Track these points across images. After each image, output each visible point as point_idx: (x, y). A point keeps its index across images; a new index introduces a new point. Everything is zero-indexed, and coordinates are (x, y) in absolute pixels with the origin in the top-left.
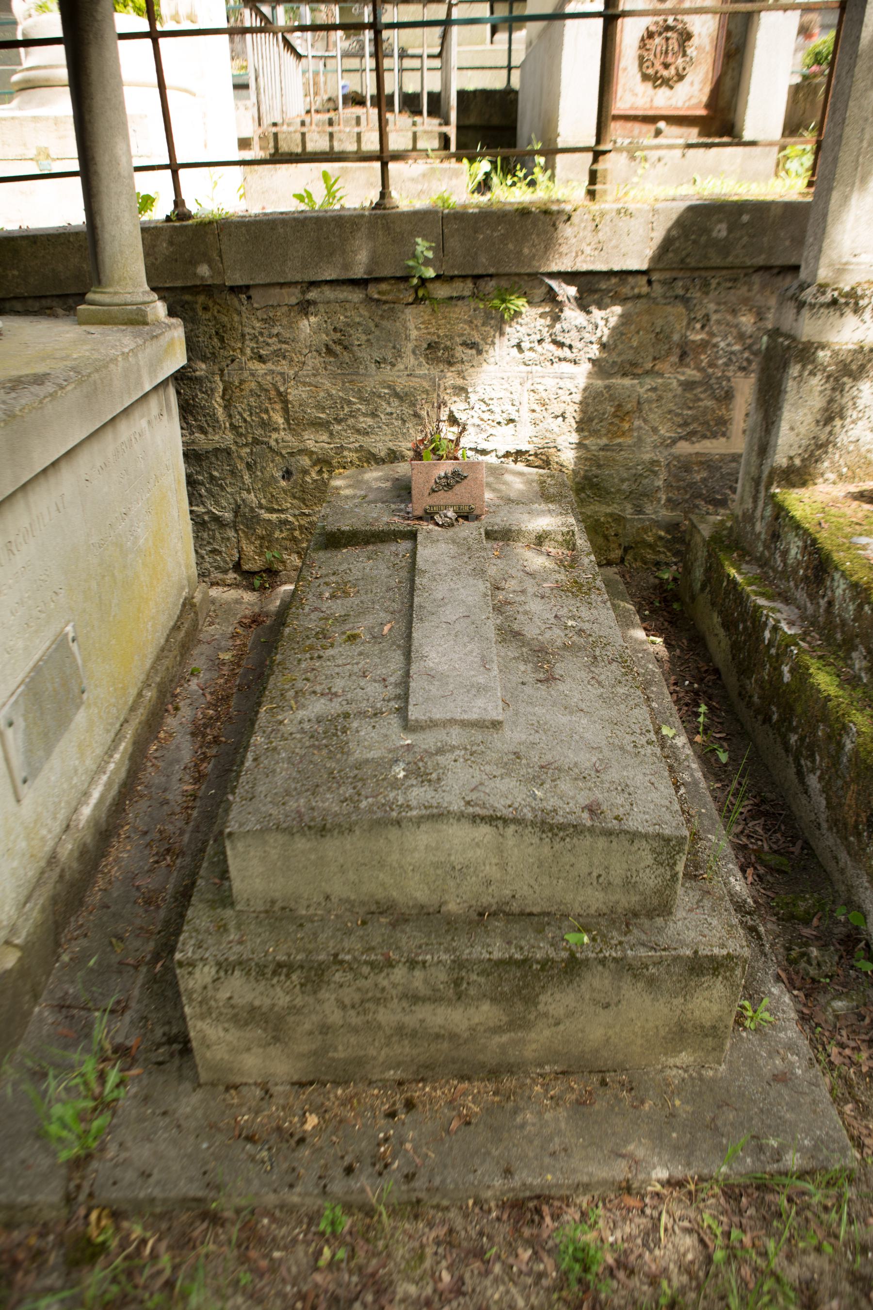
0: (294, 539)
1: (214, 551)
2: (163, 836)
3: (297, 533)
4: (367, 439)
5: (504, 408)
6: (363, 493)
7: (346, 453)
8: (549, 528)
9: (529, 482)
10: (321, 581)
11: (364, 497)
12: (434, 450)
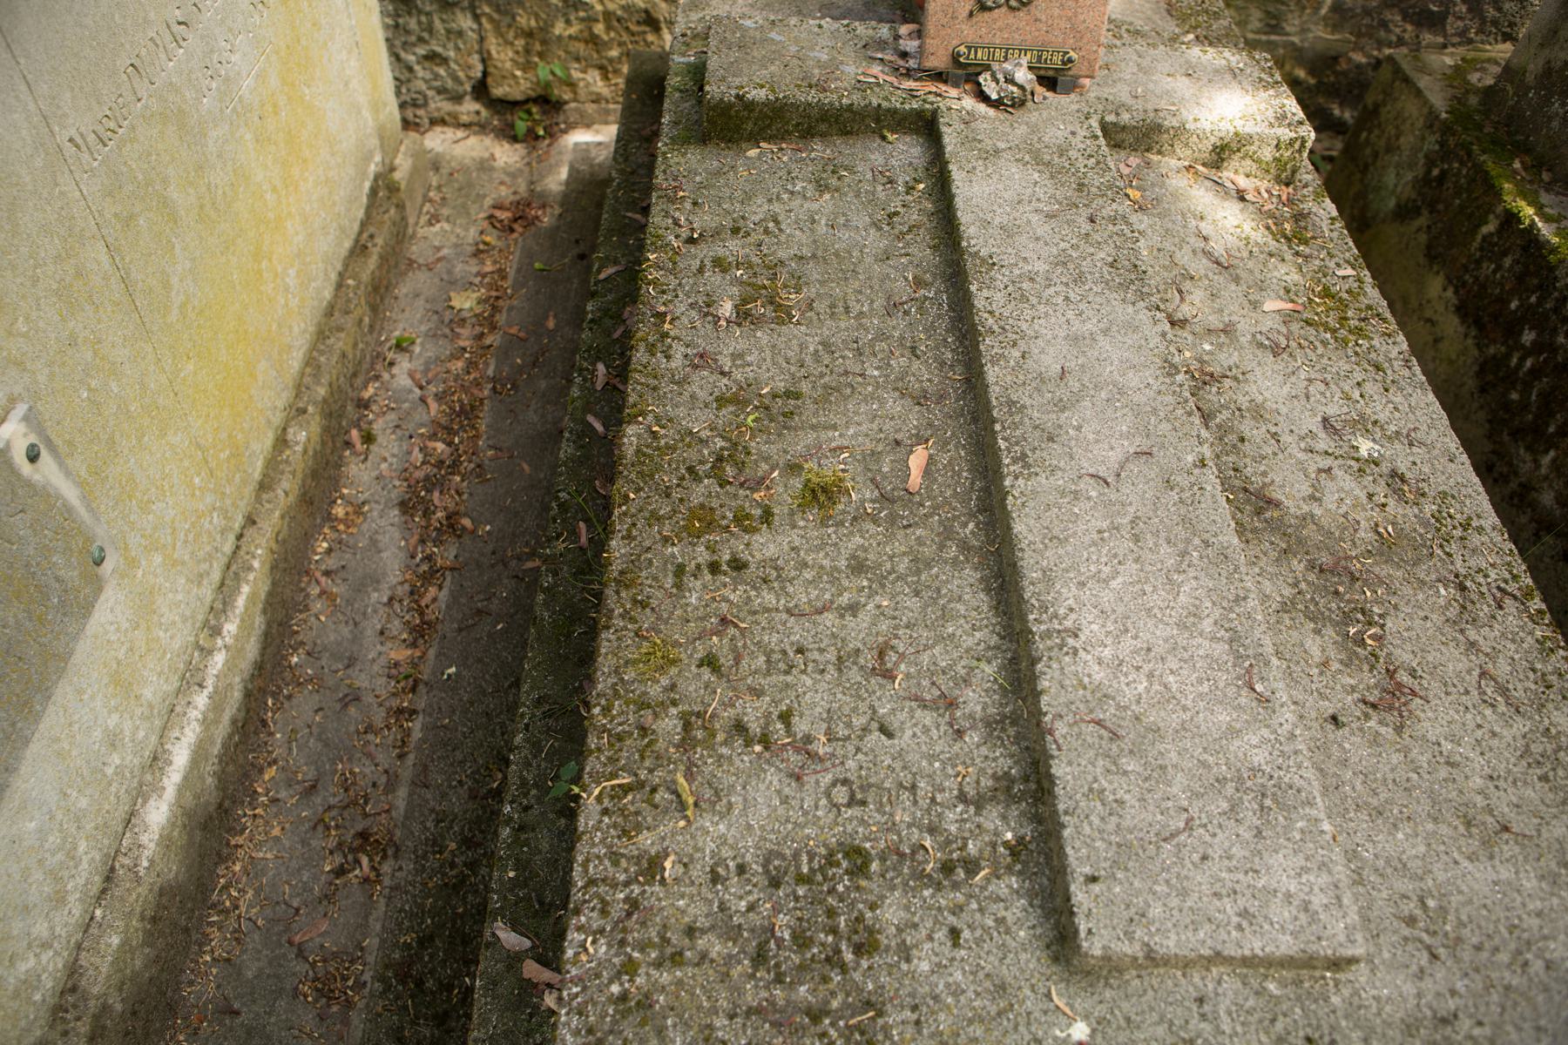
0: (593, 40)
1: (432, 57)
2: (355, 802)
3: (599, 29)
10: (704, 252)
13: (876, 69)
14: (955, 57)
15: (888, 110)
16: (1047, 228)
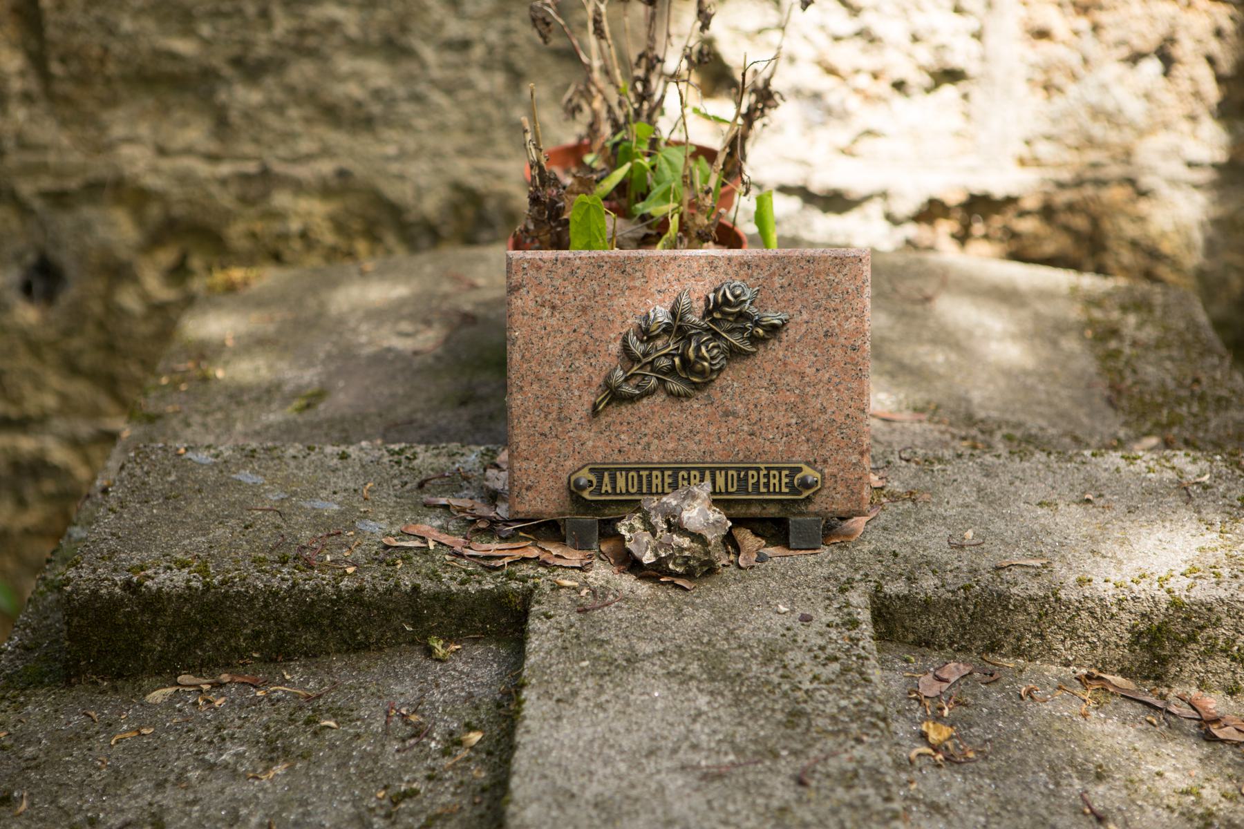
4: (365, 145)
5: (920, 22)
6: (310, 376)
7: (282, 199)
8: (1204, 591)
9: (1047, 332)
11: (313, 399)
12: (625, 198)
13: (430, 526)
14: (574, 492)
15: (436, 597)
16: (698, 800)
